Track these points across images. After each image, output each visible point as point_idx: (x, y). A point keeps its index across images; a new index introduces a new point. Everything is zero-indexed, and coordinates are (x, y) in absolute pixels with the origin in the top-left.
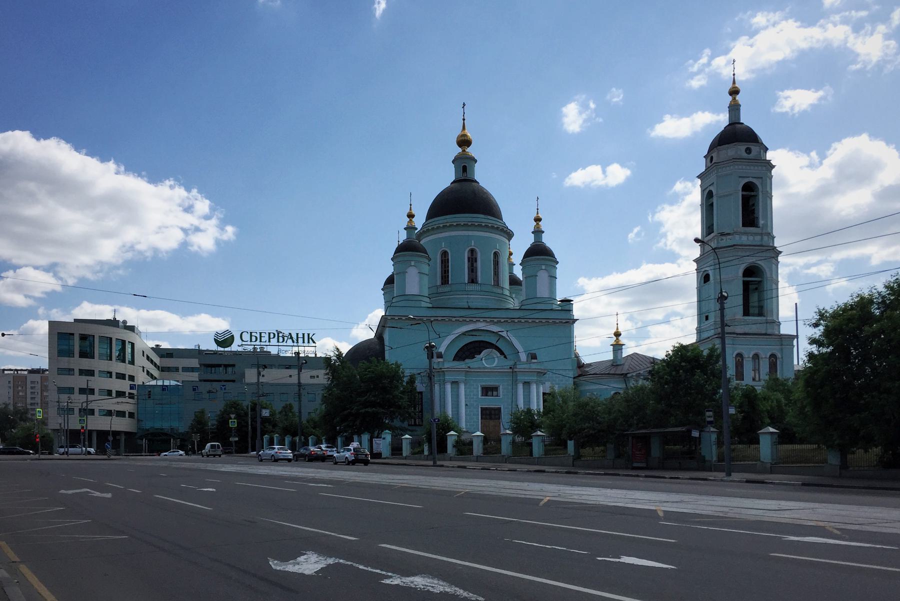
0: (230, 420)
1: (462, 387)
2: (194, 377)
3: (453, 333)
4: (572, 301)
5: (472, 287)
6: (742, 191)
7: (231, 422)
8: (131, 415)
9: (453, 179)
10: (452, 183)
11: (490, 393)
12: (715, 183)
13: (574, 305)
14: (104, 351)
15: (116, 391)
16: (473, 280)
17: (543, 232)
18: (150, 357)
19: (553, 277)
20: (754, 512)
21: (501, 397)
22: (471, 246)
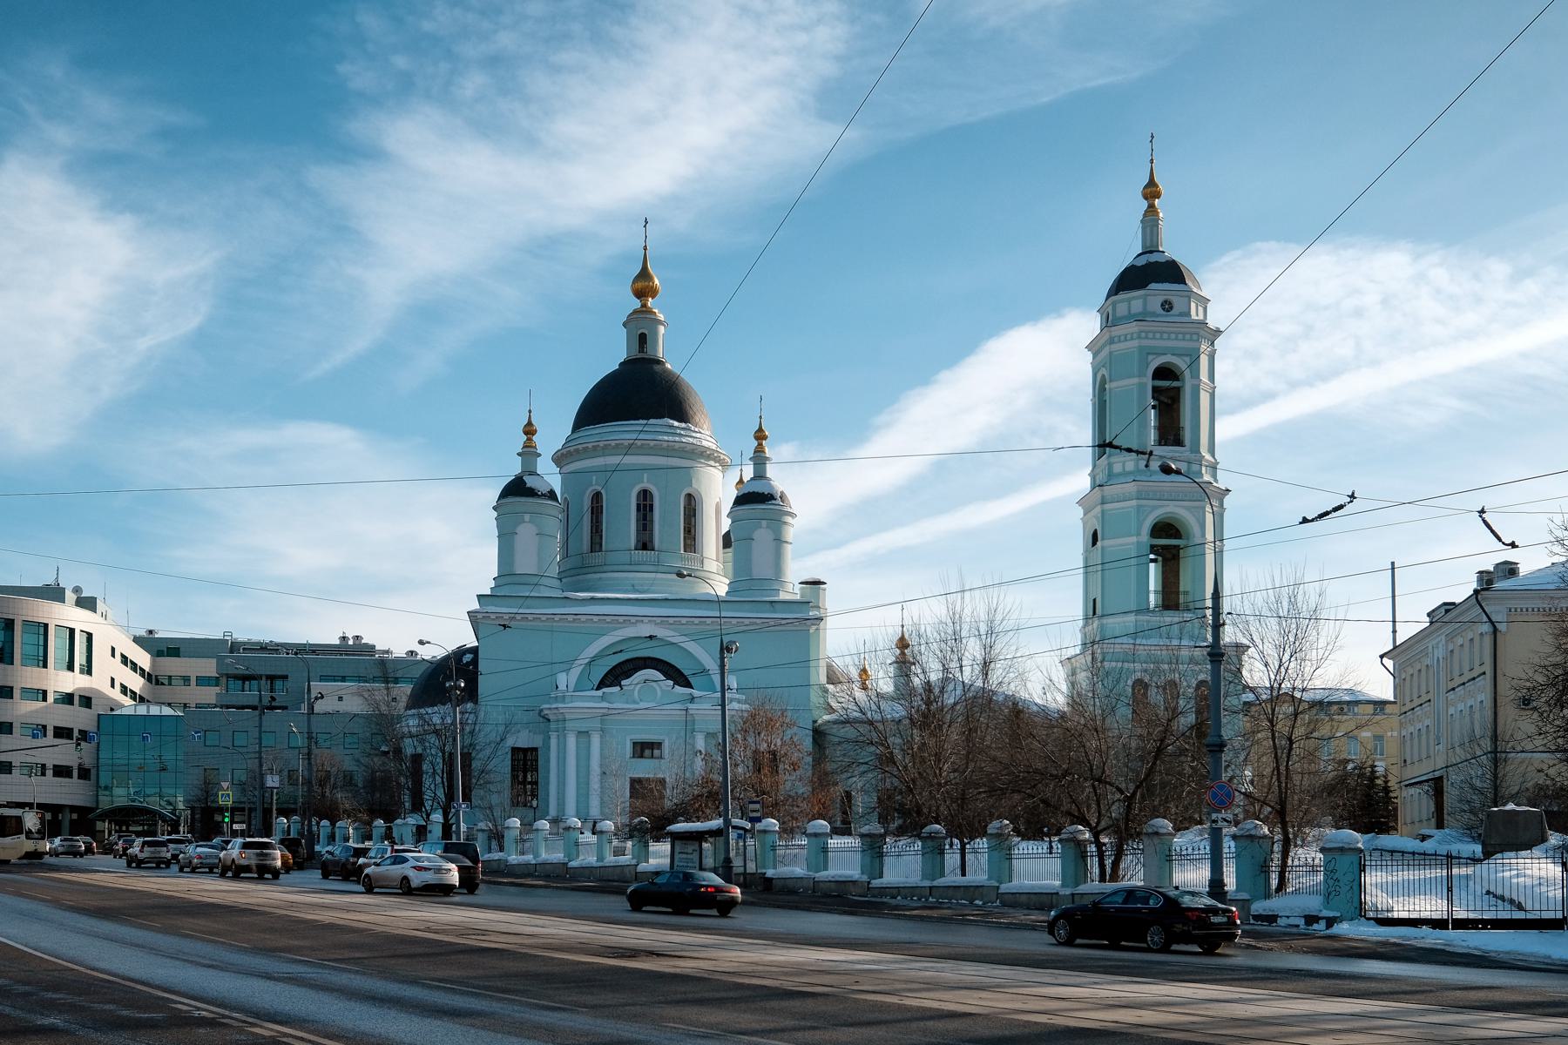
0: (220, 793)
1: (596, 740)
2: (209, 694)
6: (1153, 379)
7: (223, 795)
8: (84, 773)
11: (647, 752)
13: (827, 591)
14: (31, 650)
15: (55, 727)
16: (645, 545)
17: (540, 455)
18: (130, 657)
19: (779, 541)
20: (502, 938)
22: (643, 482)
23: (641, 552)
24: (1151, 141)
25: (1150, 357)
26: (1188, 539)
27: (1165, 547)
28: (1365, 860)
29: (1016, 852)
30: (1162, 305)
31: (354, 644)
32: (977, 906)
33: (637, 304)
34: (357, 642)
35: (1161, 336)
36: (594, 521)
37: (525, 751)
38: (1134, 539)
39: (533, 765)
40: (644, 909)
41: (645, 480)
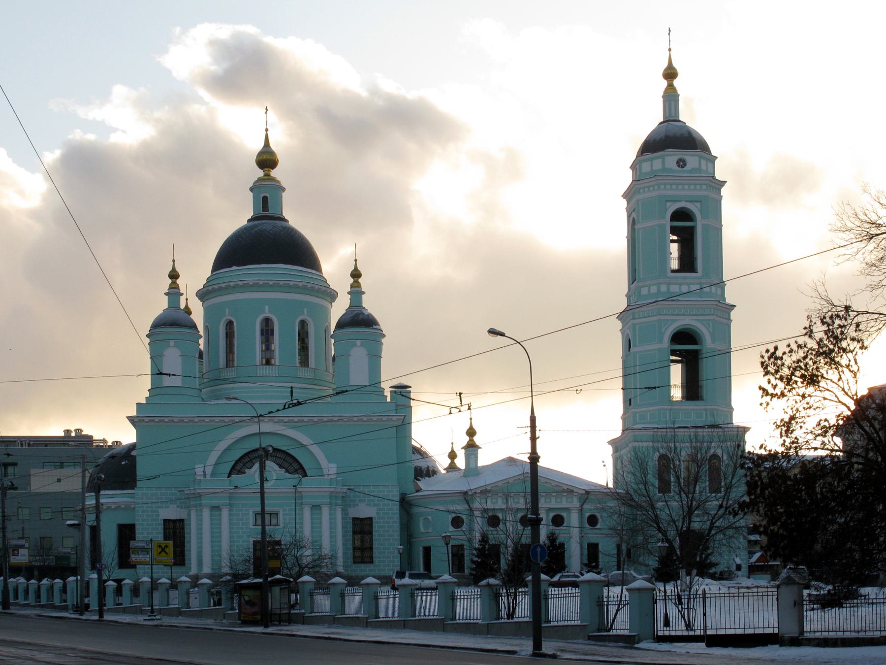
1: (225, 513)
3: (226, 438)
4: (410, 387)
5: (267, 370)
6: (671, 220)
9: (250, 215)
10: (249, 221)
12: (636, 209)
21: (281, 527)
22: (265, 313)
23: (264, 367)
24: (669, 34)
25: (668, 204)
26: (701, 344)
27: (687, 351)
28: (656, 596)
29: (381, 594)
30: (678, 162)
31: (76, 436)
33: (260, 173)
34: (78, 434)
35: (665, 187)
36: (228, 343)
37: (174, 521)
38: (656, 346)
39: (180, 533)
41: (227, 314)
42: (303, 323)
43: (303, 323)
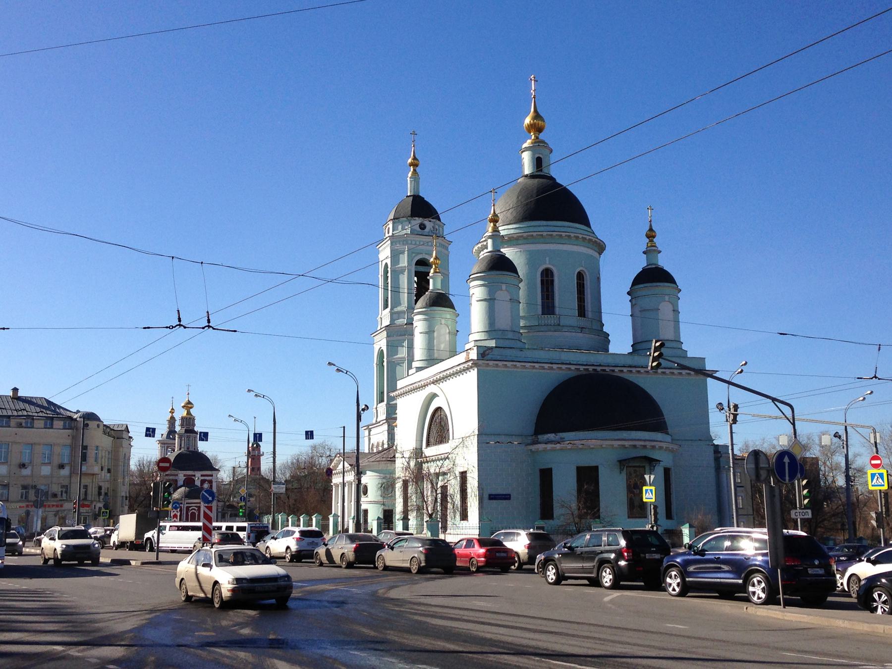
17: (660, 252)
22: (545, 263)
32: (153, 509)
40: (303, 561)
41: (547, 262)
42: (580, 276)
43: (580, 276)
